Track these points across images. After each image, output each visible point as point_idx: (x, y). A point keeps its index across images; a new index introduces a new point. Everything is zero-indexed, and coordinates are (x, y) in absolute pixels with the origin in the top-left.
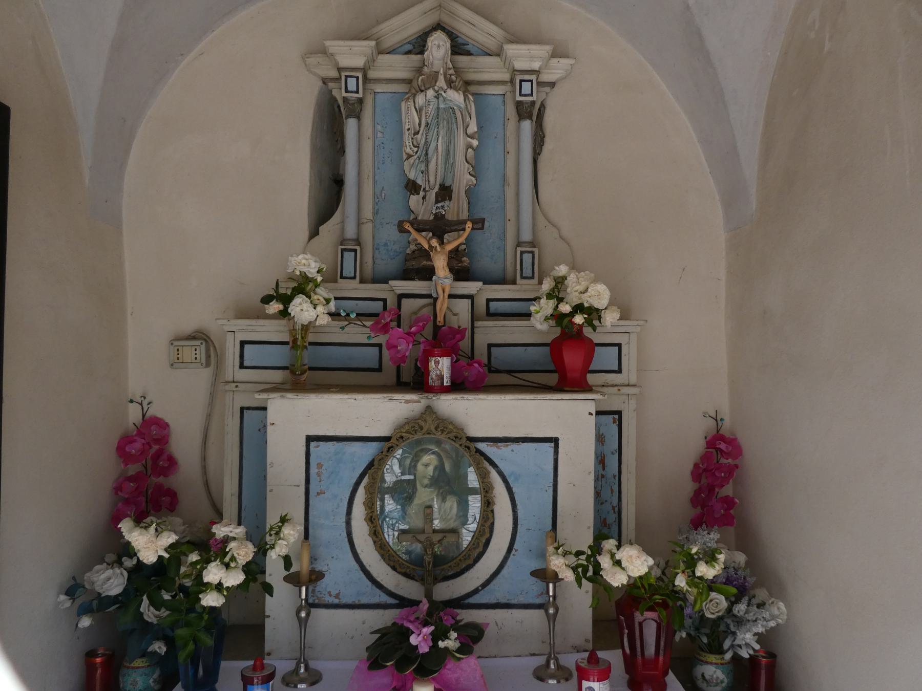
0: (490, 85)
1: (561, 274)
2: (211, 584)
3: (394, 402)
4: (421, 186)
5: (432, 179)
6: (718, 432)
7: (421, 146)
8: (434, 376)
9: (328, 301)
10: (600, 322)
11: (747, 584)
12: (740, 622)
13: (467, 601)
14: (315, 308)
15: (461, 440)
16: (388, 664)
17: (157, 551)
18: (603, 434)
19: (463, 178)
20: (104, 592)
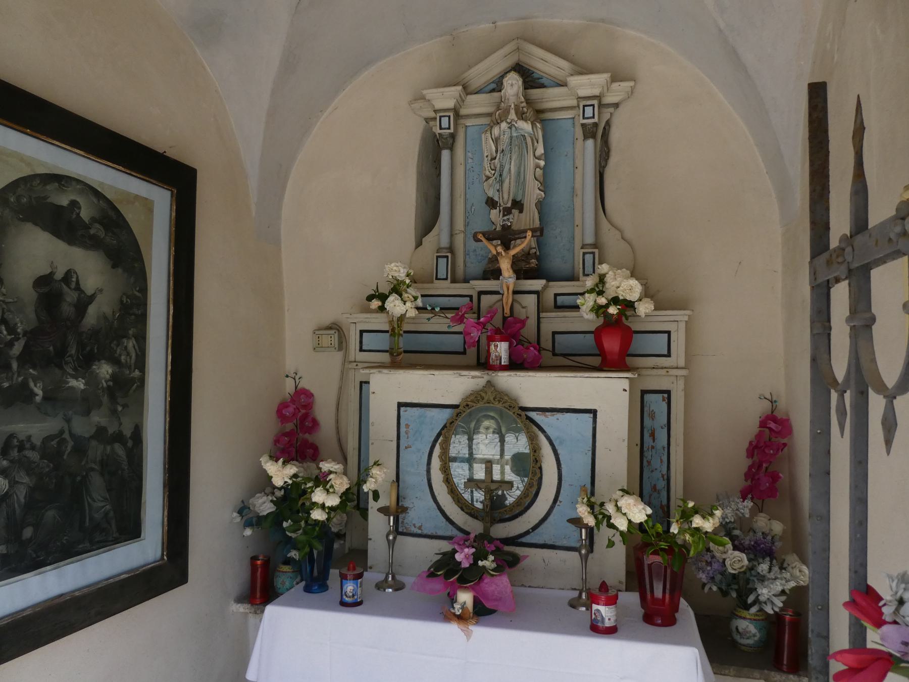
0: (560, 111)
1: (603, 272)
2: (318, 504)
3: (462, 377)
4: (497, 202)
5: (506, 196)
6: (772, 412)
7: (498, 169)
8: (494, 357)
9: (415, 298)
10: (635, 312)
11: (774, 548)
12: (762, 579)
13: (520, 540)
14: (405, 304)
15: (514, 409)
16: (439, 573)
17: (283, 478)
18: (653, 411)
19: (533, 193)
20: (261, 512)
